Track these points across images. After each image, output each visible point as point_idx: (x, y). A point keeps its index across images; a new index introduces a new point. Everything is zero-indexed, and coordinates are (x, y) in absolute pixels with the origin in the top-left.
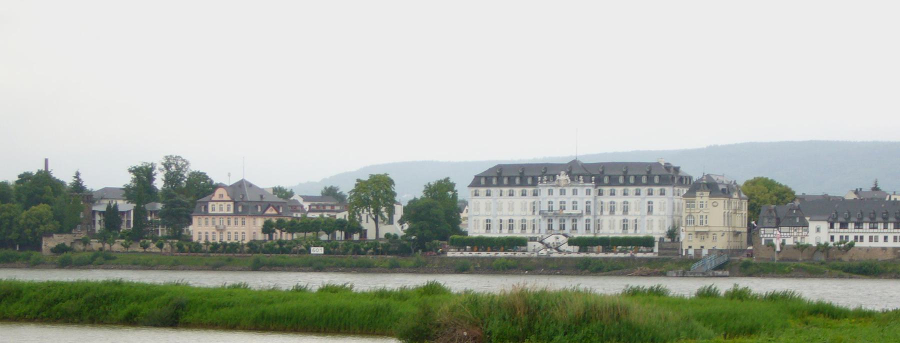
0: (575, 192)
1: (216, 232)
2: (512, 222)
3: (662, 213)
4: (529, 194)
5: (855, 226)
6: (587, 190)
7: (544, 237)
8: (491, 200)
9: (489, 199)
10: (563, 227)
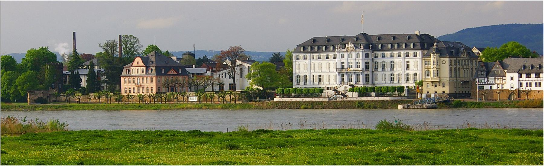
1: (135, 87)
2: (393, 76)
5: (535, 75)
6: (366, 54)
7: (338, 87)
9: (307, 61)
10: (350, 80)
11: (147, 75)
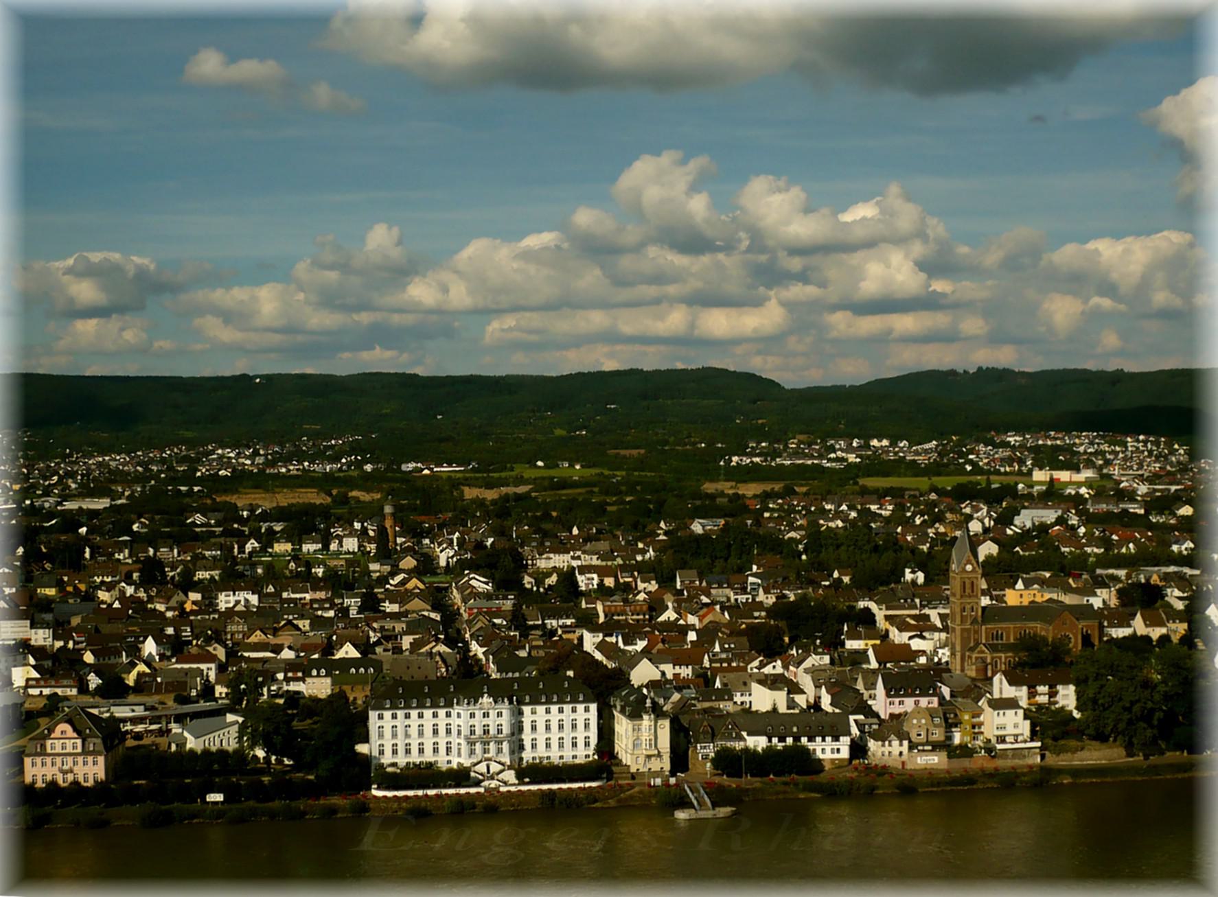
0: (561, 711)
11: (85, 752)
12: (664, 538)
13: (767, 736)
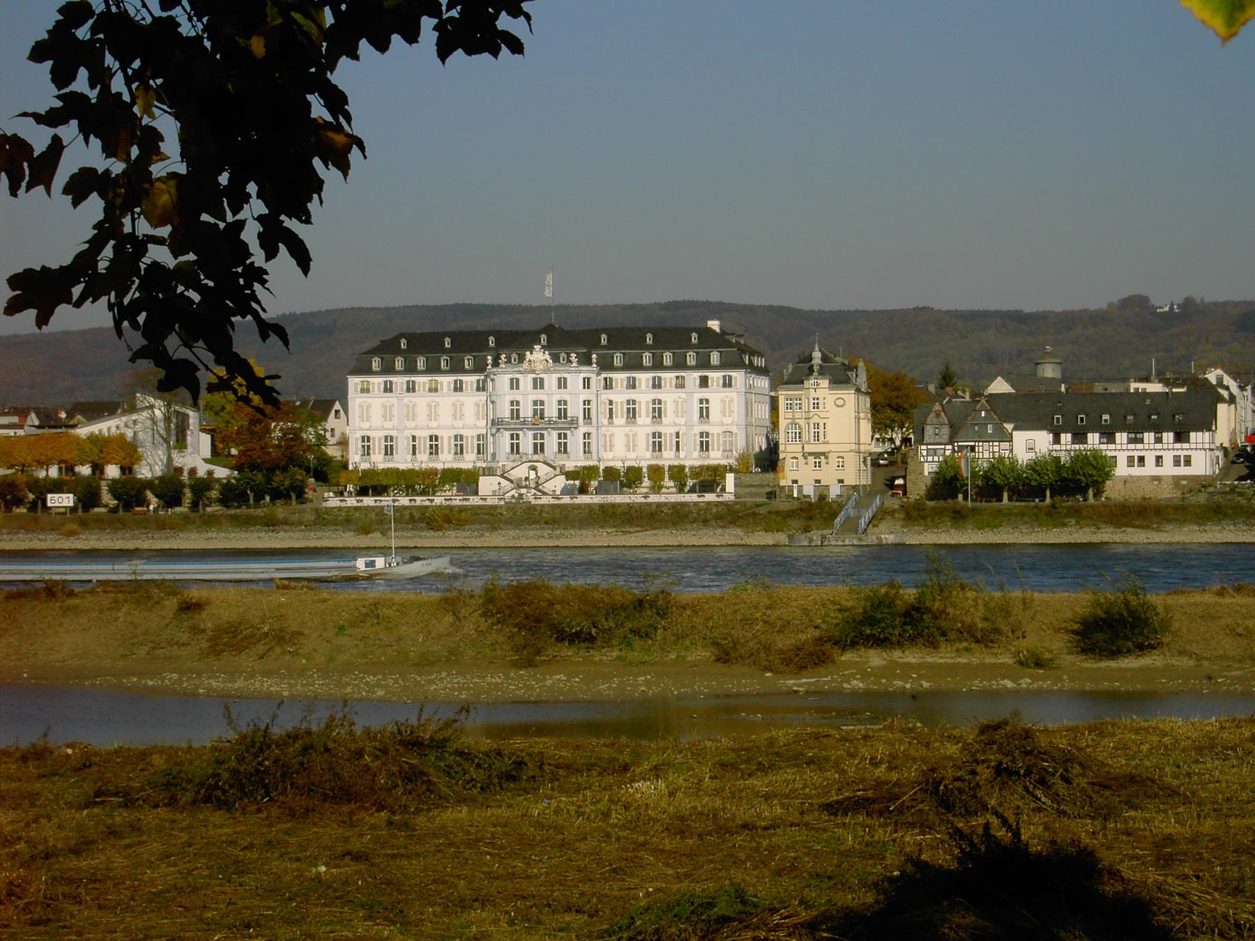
3: (728, 420)
4: (376, 388)
7: (508, 468)
8: (394, 400)
9: (391, 399)
10: (539, 448)
12: (113, 294)
13: (1050, 431)
